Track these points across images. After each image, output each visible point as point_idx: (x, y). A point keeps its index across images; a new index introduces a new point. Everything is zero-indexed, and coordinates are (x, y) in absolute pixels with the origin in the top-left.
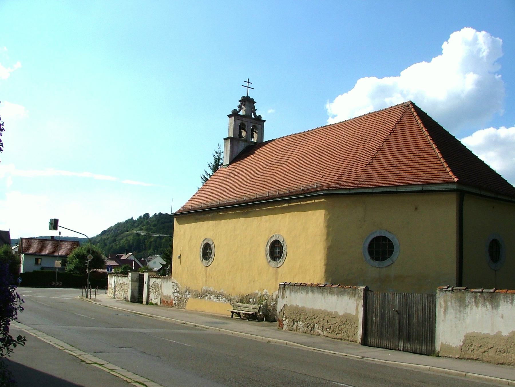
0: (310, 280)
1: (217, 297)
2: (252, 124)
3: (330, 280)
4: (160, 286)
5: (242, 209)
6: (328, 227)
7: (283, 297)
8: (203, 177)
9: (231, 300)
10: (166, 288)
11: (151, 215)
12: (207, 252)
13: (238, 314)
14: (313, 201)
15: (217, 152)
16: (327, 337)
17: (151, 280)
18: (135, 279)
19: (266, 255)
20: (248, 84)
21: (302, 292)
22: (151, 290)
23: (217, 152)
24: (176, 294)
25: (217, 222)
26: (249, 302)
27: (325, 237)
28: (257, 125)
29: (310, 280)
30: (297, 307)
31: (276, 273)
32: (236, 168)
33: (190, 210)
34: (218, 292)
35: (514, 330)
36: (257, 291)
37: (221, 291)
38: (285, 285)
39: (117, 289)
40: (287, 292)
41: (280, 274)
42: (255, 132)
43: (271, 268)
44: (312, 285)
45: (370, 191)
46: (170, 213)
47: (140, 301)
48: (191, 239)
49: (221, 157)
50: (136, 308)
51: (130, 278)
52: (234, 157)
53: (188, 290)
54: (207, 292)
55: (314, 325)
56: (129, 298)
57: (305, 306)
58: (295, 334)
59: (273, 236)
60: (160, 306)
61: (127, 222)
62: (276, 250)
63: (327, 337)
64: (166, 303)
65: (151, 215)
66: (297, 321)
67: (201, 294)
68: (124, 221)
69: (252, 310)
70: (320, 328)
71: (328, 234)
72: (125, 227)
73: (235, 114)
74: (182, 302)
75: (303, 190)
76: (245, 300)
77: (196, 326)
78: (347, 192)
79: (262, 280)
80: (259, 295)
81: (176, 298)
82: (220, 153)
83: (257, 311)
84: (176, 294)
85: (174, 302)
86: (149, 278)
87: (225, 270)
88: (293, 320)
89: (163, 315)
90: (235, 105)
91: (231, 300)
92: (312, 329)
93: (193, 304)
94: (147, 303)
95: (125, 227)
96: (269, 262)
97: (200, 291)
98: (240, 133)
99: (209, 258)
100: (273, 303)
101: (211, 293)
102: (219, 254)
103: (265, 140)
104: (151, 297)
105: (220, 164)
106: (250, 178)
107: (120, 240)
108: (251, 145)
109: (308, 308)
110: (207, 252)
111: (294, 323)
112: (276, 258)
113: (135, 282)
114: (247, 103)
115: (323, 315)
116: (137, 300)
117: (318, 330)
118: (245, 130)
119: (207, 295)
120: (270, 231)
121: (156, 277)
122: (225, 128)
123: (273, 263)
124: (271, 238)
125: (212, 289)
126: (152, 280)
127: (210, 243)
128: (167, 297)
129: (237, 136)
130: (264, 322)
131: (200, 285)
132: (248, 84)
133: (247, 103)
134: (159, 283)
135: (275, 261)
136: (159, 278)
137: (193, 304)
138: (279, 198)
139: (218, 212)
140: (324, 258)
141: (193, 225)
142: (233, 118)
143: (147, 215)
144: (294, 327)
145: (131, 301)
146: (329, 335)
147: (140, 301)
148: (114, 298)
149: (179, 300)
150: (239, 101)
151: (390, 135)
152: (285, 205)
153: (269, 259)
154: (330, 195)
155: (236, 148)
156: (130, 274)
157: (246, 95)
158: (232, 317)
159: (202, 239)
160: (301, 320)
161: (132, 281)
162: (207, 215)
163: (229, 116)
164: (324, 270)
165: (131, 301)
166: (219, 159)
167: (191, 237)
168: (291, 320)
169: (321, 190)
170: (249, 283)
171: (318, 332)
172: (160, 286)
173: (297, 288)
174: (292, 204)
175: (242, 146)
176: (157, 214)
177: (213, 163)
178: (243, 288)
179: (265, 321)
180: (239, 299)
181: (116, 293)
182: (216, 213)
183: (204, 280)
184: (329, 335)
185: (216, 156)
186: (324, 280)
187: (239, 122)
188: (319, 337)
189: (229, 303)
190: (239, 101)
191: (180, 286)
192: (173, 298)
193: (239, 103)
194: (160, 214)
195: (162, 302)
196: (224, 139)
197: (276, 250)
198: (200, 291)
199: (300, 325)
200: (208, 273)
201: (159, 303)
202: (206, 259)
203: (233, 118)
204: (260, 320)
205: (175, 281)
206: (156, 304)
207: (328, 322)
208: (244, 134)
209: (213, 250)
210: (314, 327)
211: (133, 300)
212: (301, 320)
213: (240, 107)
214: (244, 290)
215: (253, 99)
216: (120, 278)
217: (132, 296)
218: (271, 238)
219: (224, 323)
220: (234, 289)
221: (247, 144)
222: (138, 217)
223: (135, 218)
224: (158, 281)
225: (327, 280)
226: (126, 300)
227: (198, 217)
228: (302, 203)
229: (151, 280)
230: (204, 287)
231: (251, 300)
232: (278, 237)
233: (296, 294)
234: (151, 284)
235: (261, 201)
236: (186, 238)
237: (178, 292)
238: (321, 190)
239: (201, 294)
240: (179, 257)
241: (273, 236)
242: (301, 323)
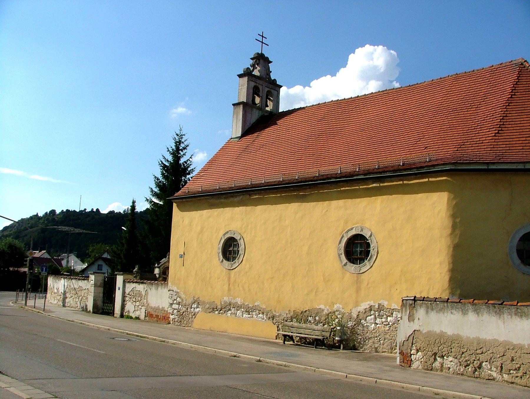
0: (421, 292)
1: (248, 311)
2: (267, 89)
3: (458, 292)
4: (143, 293)
5: (294, 191)
6: (454, 216)
7: (411, 318)
8: (160, 163)
9: (273, 318)
10: (158, 297)
11: (58, 212)
12: (230, 249)
13: (291, 338)
14: (427, 180)
15: (177, 135)
16: (512, 383)
17: (127, 285)
18: (99, 284)
19: (339, 255)
20: (262, 39)
21: (454, 311)
22: (127, 299)
23: (177, 135)
24: (175, 306)
25: (249, 208)
26: (306, 321)
27: (449, 231)
28: (272, 91)
29: (421, 292)
30: (442, 335)
31: (358, 283)
32: (254, 141)
33: (202, 192)
34: (251, 305)
35: (6, 302)
36: (322, 307)
37: (256, 304)
38: (415, 300)
39: (68, 295)
40: (421, 312)
41: (365, 284)
42: (270, 99)
43: (348, 275)
44: (435, 300)
45: (520, 166)
46: (78, 211)
47: (110, 313)
48: (201, 231)
49: (183, 140)
50: (102, 322)
51: (93, 282)
52: (247, 128)
53: (197, 302)
54: (230, 304)
55: (481, 364)
56: (90, 308)
57: (461, 333)
58: (435, 375)
59: (352, 229)
60: (143, 321)
61: (31, 218)
62: (357, 249)
63: (512, 383)
64: (156, 317)
65: (58, 212)
66: (442, 357)
67: (219, 307)
68: (29, 217)
69: (317, 333)
70: (494, 369)
71: (454, 227)
72: (28, 224)
73: (247, 73)
74: (184, 317)
75: (403, 164)
76: (301, 317)
77: (260, 361)
78: (484, 167)
79: (335, 292)
80: (326, 312)
81: (175, 311)
82: (182, 135)
83: (327, 334)
84: (175, 306)
85: (172, 317)
86: (124, 282)
87: (254, 273)
88: (435, 354)
89: (152, 332)
90: (248, 63)
91: (273, 318)
92: (476, 370)
93: (203, 321)
94: (122, 316)
95: (28, 224)
96: (345, 265)
97: (219, 304)
98: (254, 99)
99: (234, 258)
100: (350, 324)
101: (238, 307)
102: (252, 253)
103: (282, 108)
104: (127, 308)
105: (181, 148)
106: (274, 156)
107: (24, 236)
108: (266, 114)
109: (468, 338)
110: (230, 249)
111: (435, 359)
112: (356, 259)
113: (99, 286)
114: (261, 61)
115: (501, 350)
116: (101, 311)
117: (490, 370)
118: (258, 96)
119: (230, 310)
120: (346, 222)
121: (136, 282)
122: (240, 91)
123: (352, 267)
124: (347, 232)
125: (239, 301)
126: (130, 287)
127: (237, 237)
128: (157, 309)
129: (251, 102)
130: (341, 351)
131: (218, 293)
132: (262, 39)
133: (261, 61)
134: (142, 290)
135: (354, 263)
136: (142, 283)
137: (203, 321)
138: (365, 175)
139: (250, 195)
140: (447, 261)
141: (206, 213)
142: (246, 79)
143: (53, 212)
144: (437, 364)
145: (94, 312)
146: (518, 380)
147: (110, 313)
148: (64, 306)
149: (181, 315)
150: (252, 59)
151: (511, 97)
152: (374, 185)
153: (345, 260)
154: (455, 172)
155: (249, 115)
156: (92, 277)
157: (260, 52)
158: (284, 343)
159: (221, 233)
160: (453, 354)
161: (95, 285)
162: (231, 199)
163: (240, 76)
164: (447, 278)
165: (94, 312)
166: (180, 142)
167: (202, 228)
168: (430, 354)
169: (444, 164)
170: (308, 294)
171: (490, 375)
172: (143, 293)
173: (441, 305)
174: (386, 184)
175: (255, 116)
176: (65, 211)
177: (174, 148)
178: (295, 300)
179: (343, 349)
180: (289, 316)
181: (67, 300)
182: (248, 196)
183: (226, 287)
184: (518, 380)
185: (177, 139)
186: (448, 292)
187: (253, 84)
188: (492, 382)
189: (270, 322)
190: (252, 59)
191: (183, 296)
192: (171, 311)
193: (251, 62)
194: (68, 211)
195: (149, 315)
196: (234, 105)
197: (357, 249)
198: (219, 304)
199: (450, 362)
200: (232, 280)
201: (142, 317)
202: (228, 259)
203: (246, 79)
204: (333, 347)
205: (175, 289)
206: (138, 318)
207: (512, 360)
208: (258, 100)
209: (241, 248)
210: (480, 367)
211: (96, 310)
212: (453, 354)
213: (253, 66)
214: (298, 304)
215: (267, 58)
216: (73, 281)
217: (95, 306)
218: (347, 232)
219: (292, 355)
220: (451, 313)
221: (261, 113)
222: (44, 213)
223: (41, 214)
224: (140, 287)
225: (452, 293)
226: (85, 309)
227: (213, 201)
228: (405, 182)
229: (127, 285)
230: (226, 299)
231: (310, 319)
232: (362, 230)
233: (441, 315)
234: (127, 291)
235: (330, 179)
236: (193, 231)
237: (179, 304)
238: (444, 164)
239: (219, 307)
240: (181, 256)
241: (352, 229)
242: (450, 359)
